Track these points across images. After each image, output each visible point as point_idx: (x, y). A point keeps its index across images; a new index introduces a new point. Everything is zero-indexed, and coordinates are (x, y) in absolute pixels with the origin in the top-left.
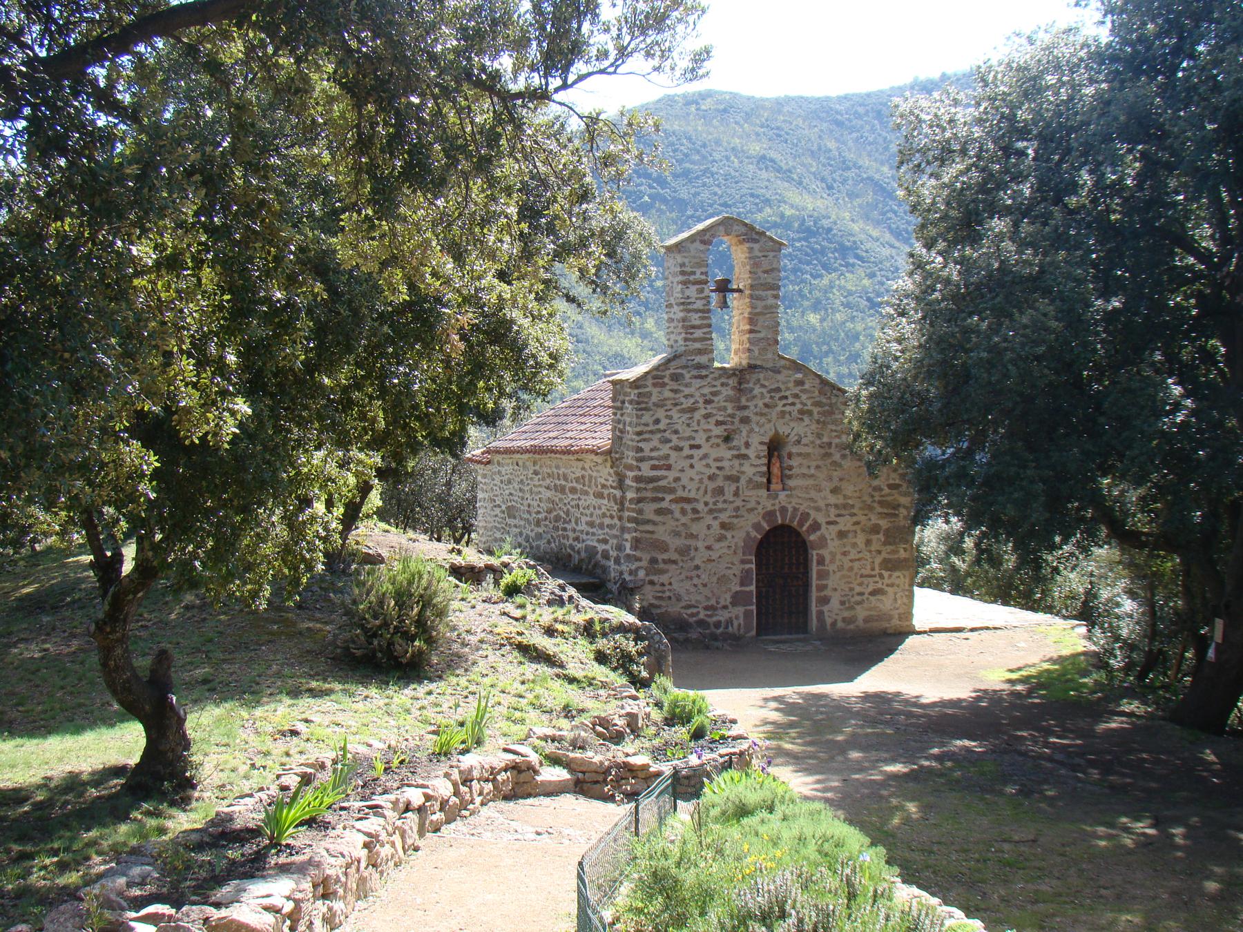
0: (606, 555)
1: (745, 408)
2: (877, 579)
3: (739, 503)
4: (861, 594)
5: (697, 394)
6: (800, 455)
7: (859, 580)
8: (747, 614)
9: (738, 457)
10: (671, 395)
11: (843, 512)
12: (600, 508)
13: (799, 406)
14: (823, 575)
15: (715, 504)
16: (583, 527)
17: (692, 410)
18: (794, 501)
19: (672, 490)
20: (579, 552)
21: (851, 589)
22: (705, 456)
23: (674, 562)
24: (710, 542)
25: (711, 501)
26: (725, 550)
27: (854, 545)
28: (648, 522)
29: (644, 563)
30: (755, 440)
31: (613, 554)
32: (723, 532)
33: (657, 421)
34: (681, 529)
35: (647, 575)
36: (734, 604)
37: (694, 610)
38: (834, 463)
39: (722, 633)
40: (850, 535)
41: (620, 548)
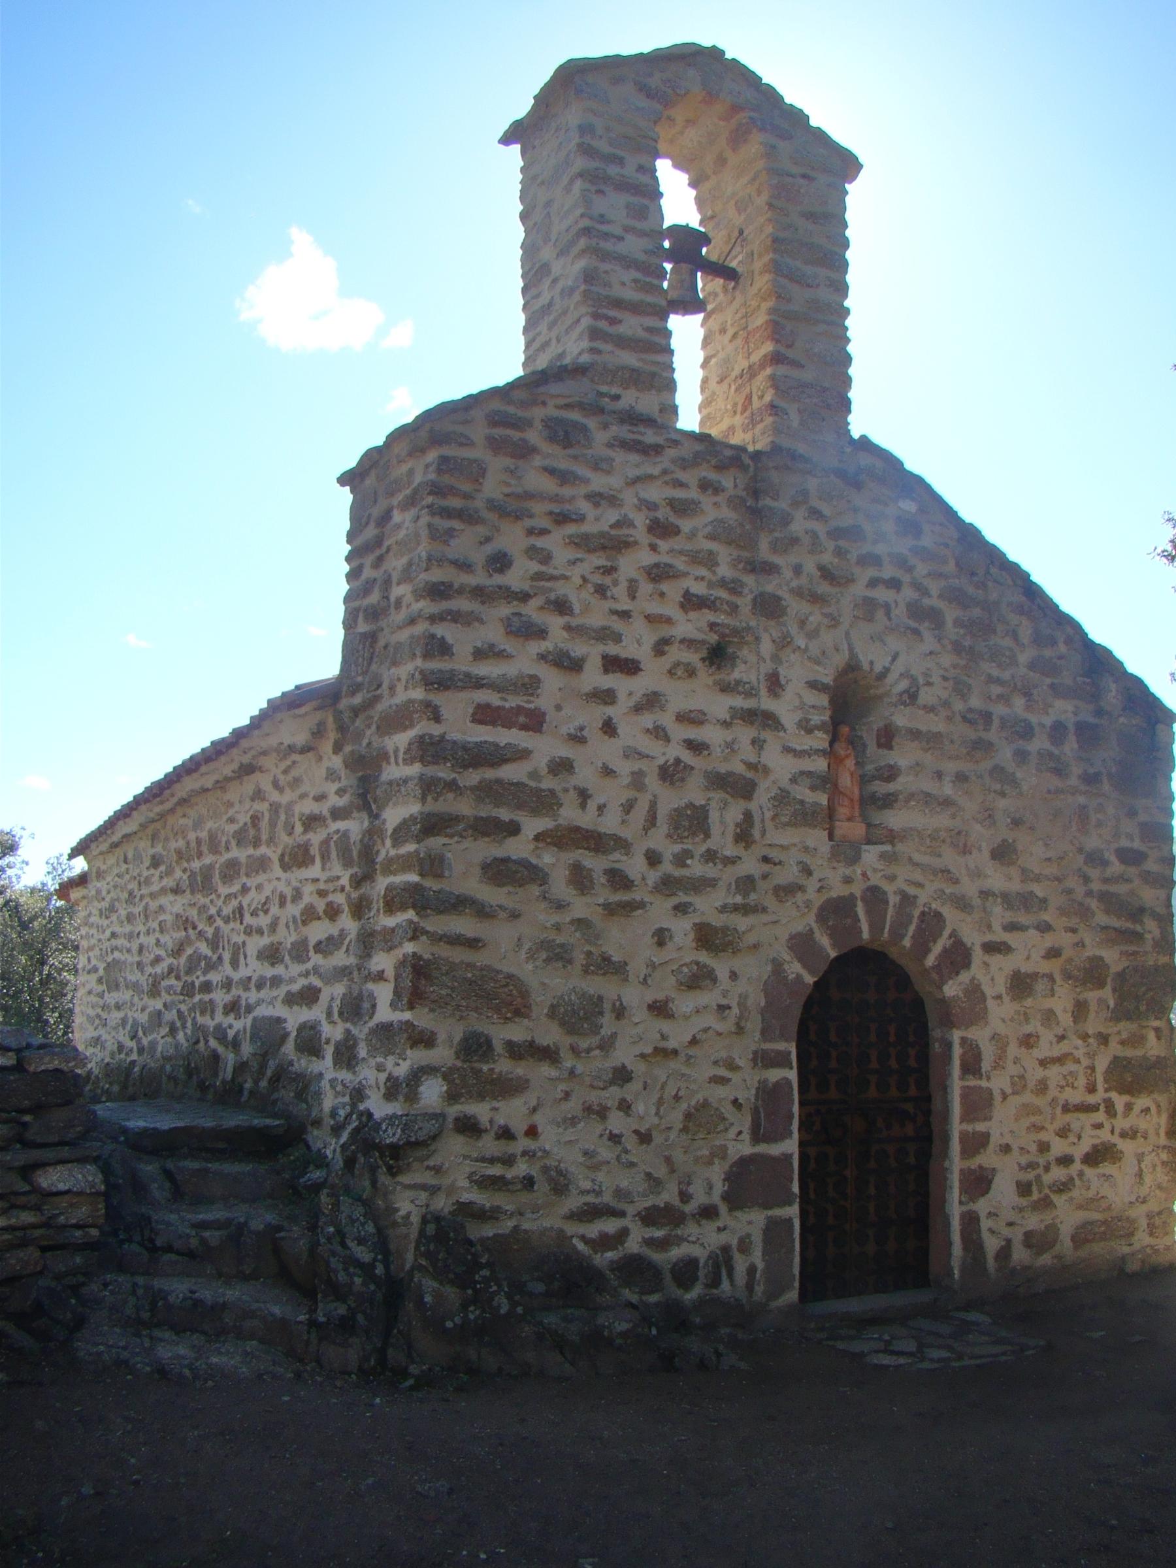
0: (310, 1043)
1: (769, 569)
2: (1100, 1116)
3: (750, 865)
4: (1065, 1161)
5: (629, 498)
6: (915, 734)
7: (1062, 1119)
8: (775, 1231)
9: (750, 716)
10: (548, 485)
11: (1023, 918)
12: (297, 895)
13: (908, 593)
14: (979, 1105)
15: (681, 860)
16: (253, 968)
17: (614, 544)
18: (903, 873)
19: (545, 802)
20: (235, 1044)
21: (1044, 1147)
22: (652, 701)
23: (548, 1054)
24: (665, 987)
25: (669, 850)
26: (710, 1020)
27: (1049, 1017)
28: (459, 904)
29: (442, 1055)
30: (795, 673)
31: (333, 1032)
32: (704, 957)
33: (500, 562)
34: (569, 937)
35: (452, 1097)
36: (735, 1199)
37: (610, 1226)
38: (998, 772)
39: (701, 1303)
40: (1041, 986)
41: (355, 1008)
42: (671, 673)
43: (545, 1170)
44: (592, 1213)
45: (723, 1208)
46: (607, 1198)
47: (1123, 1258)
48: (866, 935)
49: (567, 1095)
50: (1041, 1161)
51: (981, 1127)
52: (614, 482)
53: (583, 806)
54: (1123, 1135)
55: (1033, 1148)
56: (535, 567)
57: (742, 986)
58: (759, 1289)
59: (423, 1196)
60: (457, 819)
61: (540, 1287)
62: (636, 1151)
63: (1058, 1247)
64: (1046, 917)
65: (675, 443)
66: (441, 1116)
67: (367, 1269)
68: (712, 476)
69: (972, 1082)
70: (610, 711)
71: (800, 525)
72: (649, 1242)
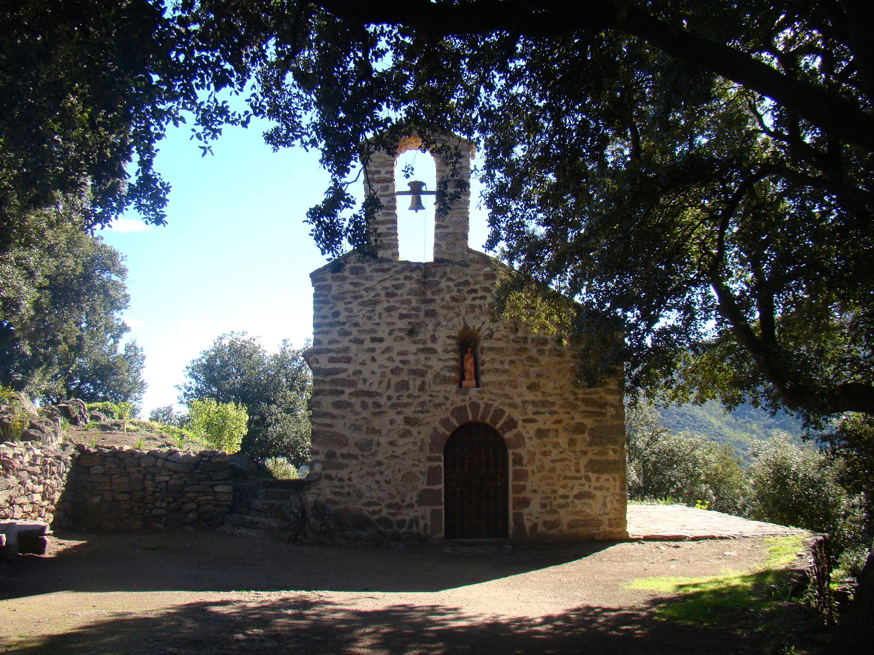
1: (431, 301)
2: (583, 481)
3: (425, 398)
4: (565, 497)
5: (379, 287)
6: (491, 349)
7: (563, 482)
8: (435, 514)
9: (423, 350)
10: (352, 288)
11: (542, 410)
14: (521, 475)
15: (398, 398)
17: (374, 303)
19: (352, 384)
22: (388, 349)
23: (355, 457)
24: (394, 437)
27: (556, 445)
28: (325, 415)
29: (321, 457)
30: (442, 334)
32: (408, 427)
33: (337, 314)
35: (324, 469)
36: (420, 503)
37: (377, 508)
38: (531, 358)
40: (551, 434)
42: (395, 340)
43: (355, 491)
44: (370, 504)
45: (416, 505)
46: (375, 500)
47: (594, 534)
48: (470, 418)
49: (361, 469)
50: (553, 496)
51: (522, 483)
52: (374, 283)
53: (365, 384)
54: (595, 488)
55: (549, 492)
56: (347, 314)
57: (422, 436)
58: (429, 532)
59: (315, 496)
60: (325, 390)
61: (351, 524)
62: (385, 486)
63: (560, 528)
64: (554, 409)
65: (395, 266)
66: (321, 474)
67: (296, 515)
68: (409, 274)
69: (518, 467)
70: (374, 354)
71: (444, 284)
72: (390, 514)
